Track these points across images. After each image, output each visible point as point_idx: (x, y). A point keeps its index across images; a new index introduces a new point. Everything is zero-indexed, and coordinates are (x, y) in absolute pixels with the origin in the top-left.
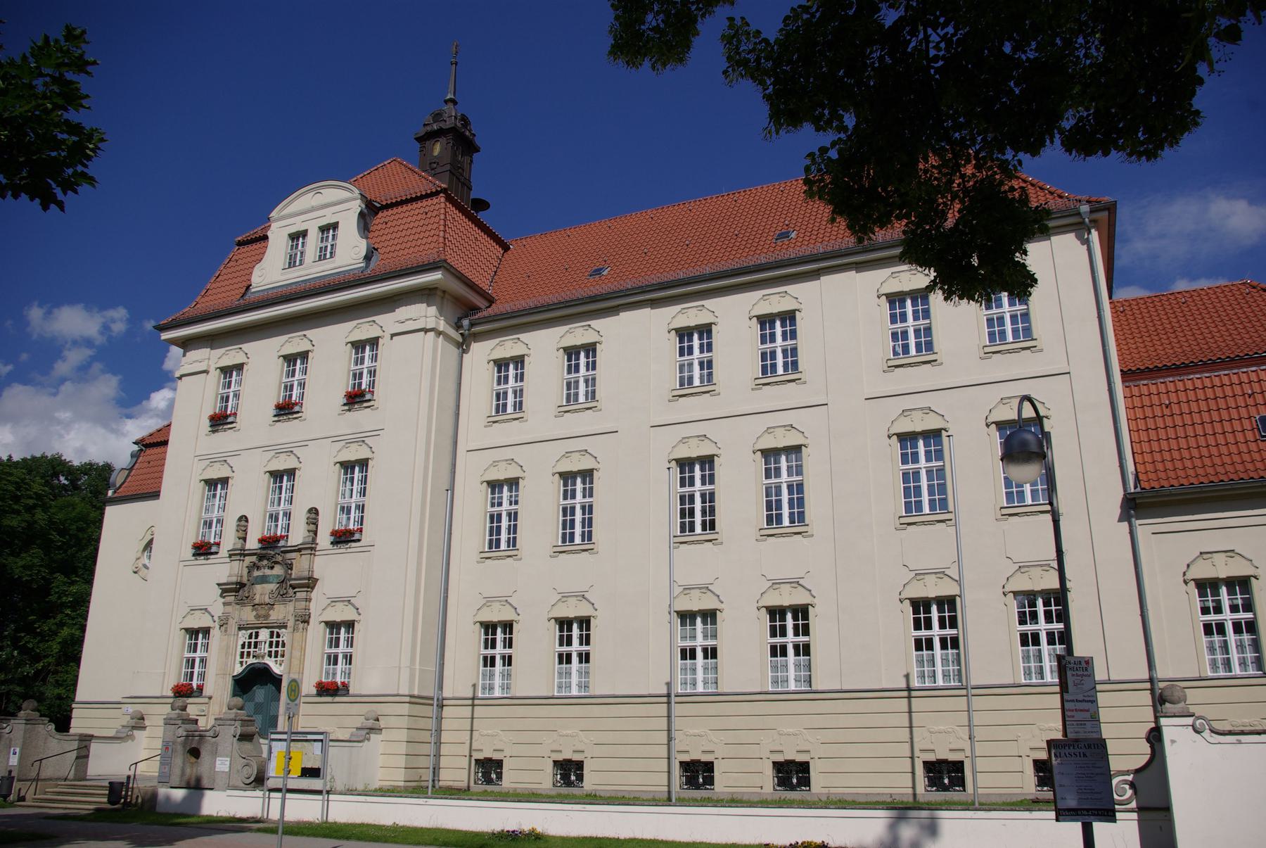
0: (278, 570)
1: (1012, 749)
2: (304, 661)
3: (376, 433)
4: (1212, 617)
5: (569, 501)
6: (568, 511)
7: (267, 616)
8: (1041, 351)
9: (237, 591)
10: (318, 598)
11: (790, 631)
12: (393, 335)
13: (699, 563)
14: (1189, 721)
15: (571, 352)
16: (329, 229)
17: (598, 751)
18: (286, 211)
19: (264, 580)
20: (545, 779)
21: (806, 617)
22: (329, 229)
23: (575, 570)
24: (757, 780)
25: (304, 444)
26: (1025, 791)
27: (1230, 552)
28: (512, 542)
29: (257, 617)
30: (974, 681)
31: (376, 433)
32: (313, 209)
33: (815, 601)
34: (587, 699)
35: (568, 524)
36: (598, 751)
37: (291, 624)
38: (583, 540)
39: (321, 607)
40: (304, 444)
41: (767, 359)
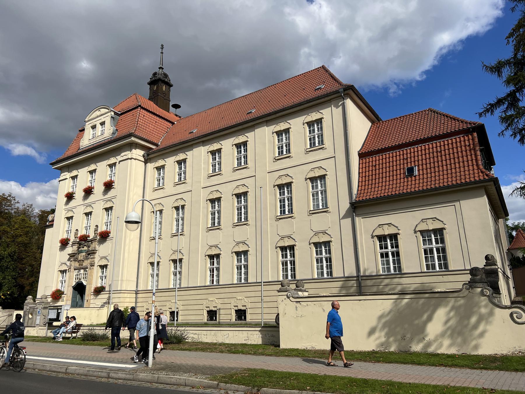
0: (86, 248)
1: (201, 307)
2: (93, 280)
3: (115, 197)
4: (384, 250)
5: (282, 197)
6: (282, 201)
7: (82, 265)
8: (326, 149)
9: (74, 256)
10: (97, 256)
11: (389, 247)
12: (120, 161)
13: (216, 237)
14: (286, 293)
15: (238, 146)
16: (103, 124)
17: (253, 305)
18: (90, 118)
19: (81, 252)
20: (205, 318)
21: (396, 239)
22: (103, 124)
23: (241, 234)
24: (229, 317)
25: (75, 207)
26: (203, 321)
27: (389, 224)
28: (291, 211)
29: (79, 265)
30: (405, 271)
31: (115, 197)
32: (98, 117)
33: (446, 226)
34: (181, 289)
35: (283, 206)
36: (253, 305)
37: (89, 267)
38: (289, 212)
39: (97, 260)
40: (75, 207)
41: (312, 141)
